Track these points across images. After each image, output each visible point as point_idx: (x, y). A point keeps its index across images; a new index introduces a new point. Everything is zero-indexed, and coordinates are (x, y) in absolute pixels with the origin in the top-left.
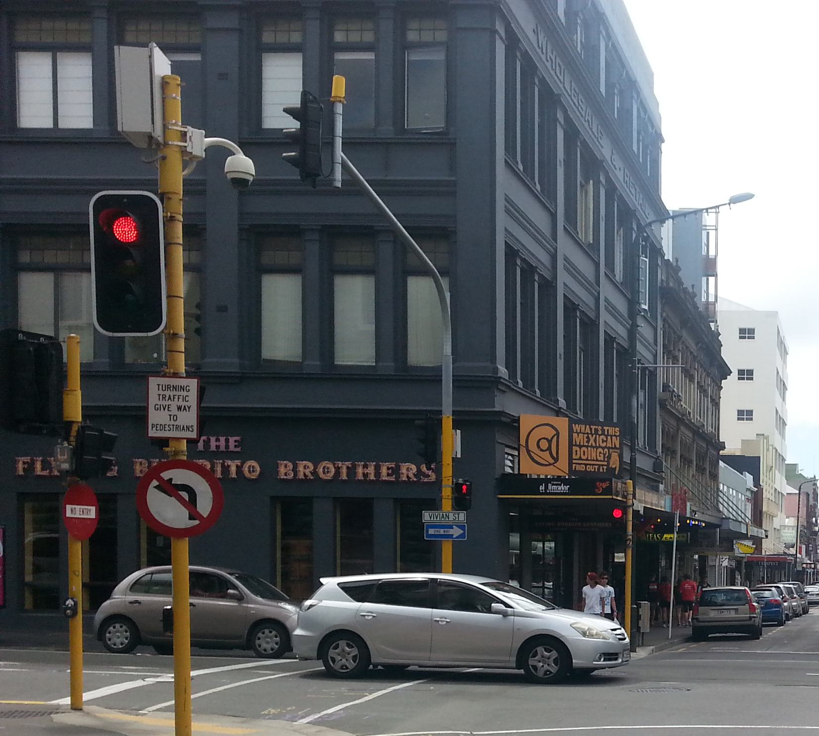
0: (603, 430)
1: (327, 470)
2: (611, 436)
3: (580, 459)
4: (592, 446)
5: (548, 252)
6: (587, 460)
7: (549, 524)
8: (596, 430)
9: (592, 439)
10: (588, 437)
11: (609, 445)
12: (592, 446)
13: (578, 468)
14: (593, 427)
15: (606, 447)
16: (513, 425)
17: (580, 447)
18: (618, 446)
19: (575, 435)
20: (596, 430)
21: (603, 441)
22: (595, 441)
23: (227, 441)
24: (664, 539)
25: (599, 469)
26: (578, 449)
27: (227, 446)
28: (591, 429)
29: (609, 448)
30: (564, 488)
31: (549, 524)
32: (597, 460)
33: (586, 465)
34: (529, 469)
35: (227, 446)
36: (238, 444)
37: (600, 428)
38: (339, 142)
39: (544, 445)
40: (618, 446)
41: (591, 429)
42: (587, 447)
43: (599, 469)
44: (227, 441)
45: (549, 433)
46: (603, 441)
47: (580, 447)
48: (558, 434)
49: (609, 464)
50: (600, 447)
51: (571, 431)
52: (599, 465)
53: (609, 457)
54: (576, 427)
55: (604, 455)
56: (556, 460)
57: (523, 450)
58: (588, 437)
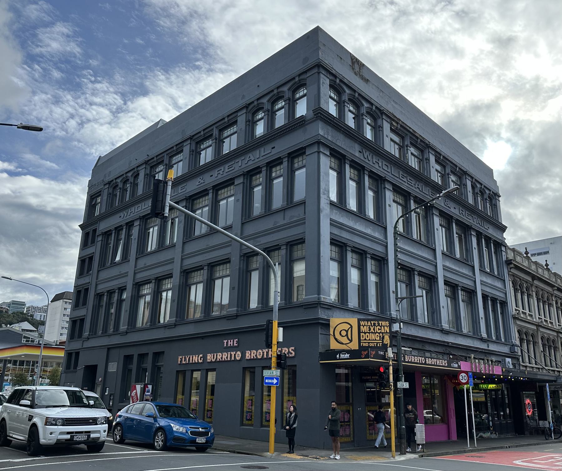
0: (379, 324)
1: (429, 361)
2: (384, 326)
3: (365, 339)
4: (372, 332)
5: (503, 293)
6: (369, 340)
7: (369, 378)
8: (374, 324)
9: (372, 329)
10: (369, 328)
11: (383, 331)
12: (372, 332)
13: (364, 345)
14: (372, 322)
15: (381, 332)
16: (326, 325)
17: (365, 333)
18: (388, 331)
19: (362, 327)
20: (374, 324)
21: (379, 329)
22: (374, 329)
23: (233, 341)
24: (489, 388)
25: (377, 345)
26: (364, 334)
27: (233, 344)
28: (371, 323)
29: (383, 333)
30: (347, 356)
31: (369, 378)
32: (376, 340)
33: (369, 343)
34: (334, 345)
35: (233, 344)
36: (237, 342)
37: (376, 322)
38: (118, 196)
39: (344, 333)
40: (388, 331)
41: (371, 323)
42: (369, 333)
43: (377, 345)
44: (233, 341)
45: (347, 327)
46: (379, 329)
47: (365, 333)
48: (351, 327)
49: (383, 342)
50: (377, 332)
51: (359, 326)
52: (377, 343)
53: (383, 338)
54: (362, 323)
55: (380, 337)
56: (351, 341)
57: (332, 338)
58: (369, 328)
